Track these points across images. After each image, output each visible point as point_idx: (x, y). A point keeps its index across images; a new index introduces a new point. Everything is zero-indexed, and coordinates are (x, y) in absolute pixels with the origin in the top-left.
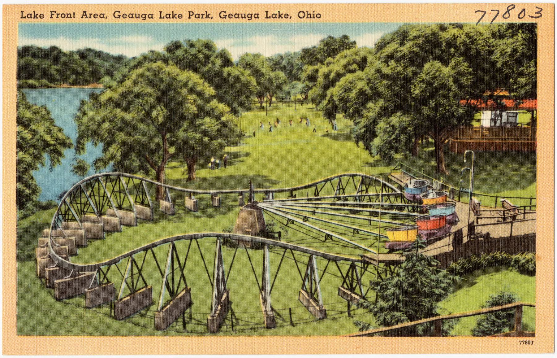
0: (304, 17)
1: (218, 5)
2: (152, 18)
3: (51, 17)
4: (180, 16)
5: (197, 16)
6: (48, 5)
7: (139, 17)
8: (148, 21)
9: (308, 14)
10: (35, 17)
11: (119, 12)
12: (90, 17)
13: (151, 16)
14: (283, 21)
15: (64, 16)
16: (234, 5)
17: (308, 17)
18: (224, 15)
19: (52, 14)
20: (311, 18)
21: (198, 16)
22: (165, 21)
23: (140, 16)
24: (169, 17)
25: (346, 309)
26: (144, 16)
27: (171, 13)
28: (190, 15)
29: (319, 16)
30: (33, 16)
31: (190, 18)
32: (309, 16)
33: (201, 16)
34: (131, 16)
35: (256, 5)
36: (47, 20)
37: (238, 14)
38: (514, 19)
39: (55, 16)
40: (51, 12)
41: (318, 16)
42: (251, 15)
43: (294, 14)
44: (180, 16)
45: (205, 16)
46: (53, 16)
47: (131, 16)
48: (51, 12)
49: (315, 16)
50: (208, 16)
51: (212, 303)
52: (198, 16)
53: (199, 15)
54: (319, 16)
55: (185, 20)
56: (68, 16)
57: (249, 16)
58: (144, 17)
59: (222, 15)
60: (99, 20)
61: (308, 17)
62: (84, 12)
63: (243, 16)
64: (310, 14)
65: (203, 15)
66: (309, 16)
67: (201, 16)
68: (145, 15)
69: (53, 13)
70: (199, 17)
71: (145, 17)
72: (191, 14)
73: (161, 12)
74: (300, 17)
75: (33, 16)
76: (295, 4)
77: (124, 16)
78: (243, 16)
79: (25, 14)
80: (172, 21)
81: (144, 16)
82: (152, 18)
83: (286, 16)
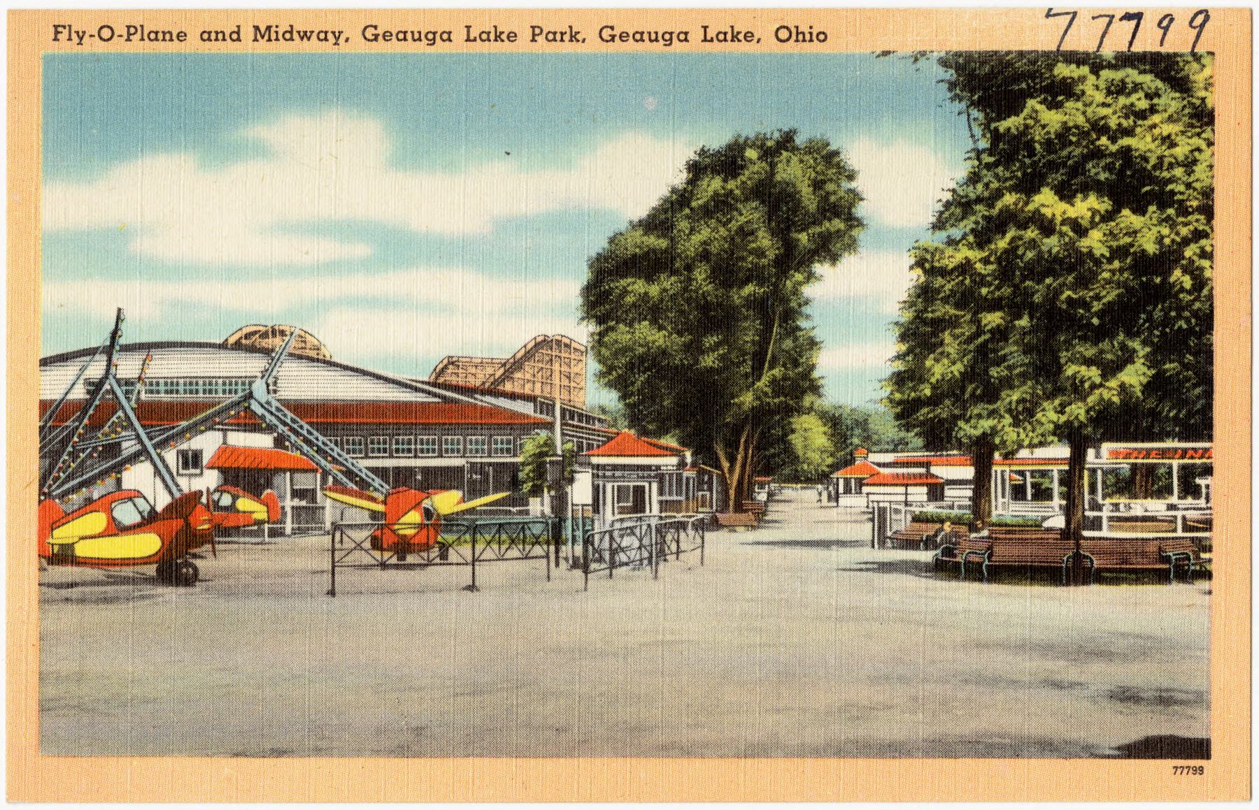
0: (788, 40)
1: (596, 12)
2: (686, 40)
3: (56, 39)
4: (512, 37)
5: (551, 37)
6: (46, 12)
7: (656, 40)
8: (441, 47)
9: (797, 33)
10: (498, 37)
11: (376, 27)
12: (562, 40)
13: (448, 37)
14: (743, 47)
15: (155, 36)
16: (394, 12)
17: (797, 41)
18: (609, 34)
19: (57, 33)
20: (804, 40)
21: (553, 37)
22: (716, 47)
23: (660, 38)
24: (725, 40)
25: (327, 566)
26: (430, 36)
27: (493, 30)
28: (534, 35)
29: (823, 37)
30: (492, 37)
31: (533, 40)
32: (801, 37)
33: (558, 37)
34: (403, 36)
35: (510, 12)
36: (523, 44)
37: (642, 33)
38: (1148, 42)
39: (63, 36)
40: (56, 27)
41: (822, 37)
42: (434, 33)
43: (765, 31)
44: (512, 37)
45: (567, 37)
46: (59, 36)
47: (403, 36)
48: (56, 27)
49: (280, 36)
50: (574, 37)
51: (861, 570)
52: (553, 37)
53: (555, 33)
54: (823, 37)
55: (247, 46)
56: (167, 36)
57: (667, 37)
58: (668, 38)
59: (606, 34)
60: (567, 47)
61: (797, 41)
62: (257, 28)
63: (416, 36)
64: (803, 33)
65: (562, 34)
66: (799, 36)
67: (558, 37)
68: (671, 34)
69: (60, 29)
70: (555, 40)
71: (671, 39)
72: (537, 31)
73: (705, 28)
74: (781, 41)
75: (729, 37)
76: (888, 10)
77: (387, 36)
78: (653, 37)
79: (711, 33)
80: (729, 47)
81: (667, 37)
82: (686, 40)
83: (749, 36)
